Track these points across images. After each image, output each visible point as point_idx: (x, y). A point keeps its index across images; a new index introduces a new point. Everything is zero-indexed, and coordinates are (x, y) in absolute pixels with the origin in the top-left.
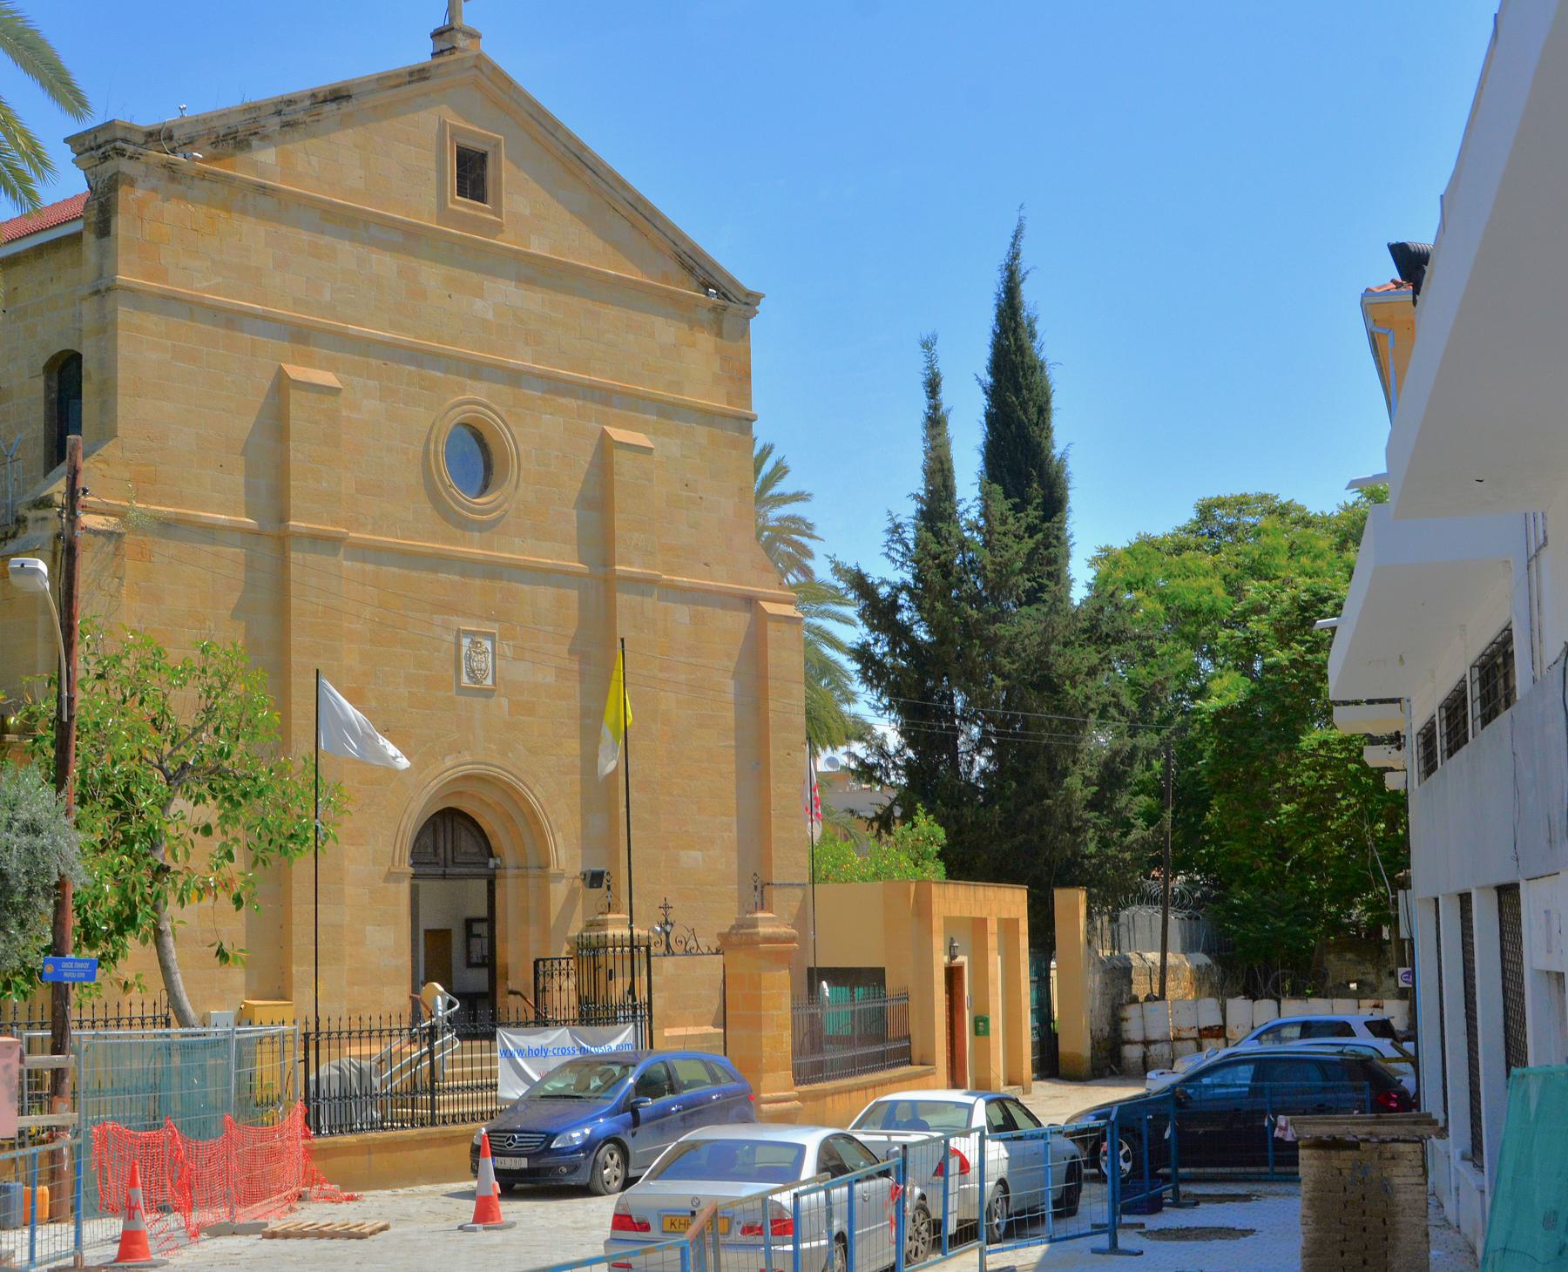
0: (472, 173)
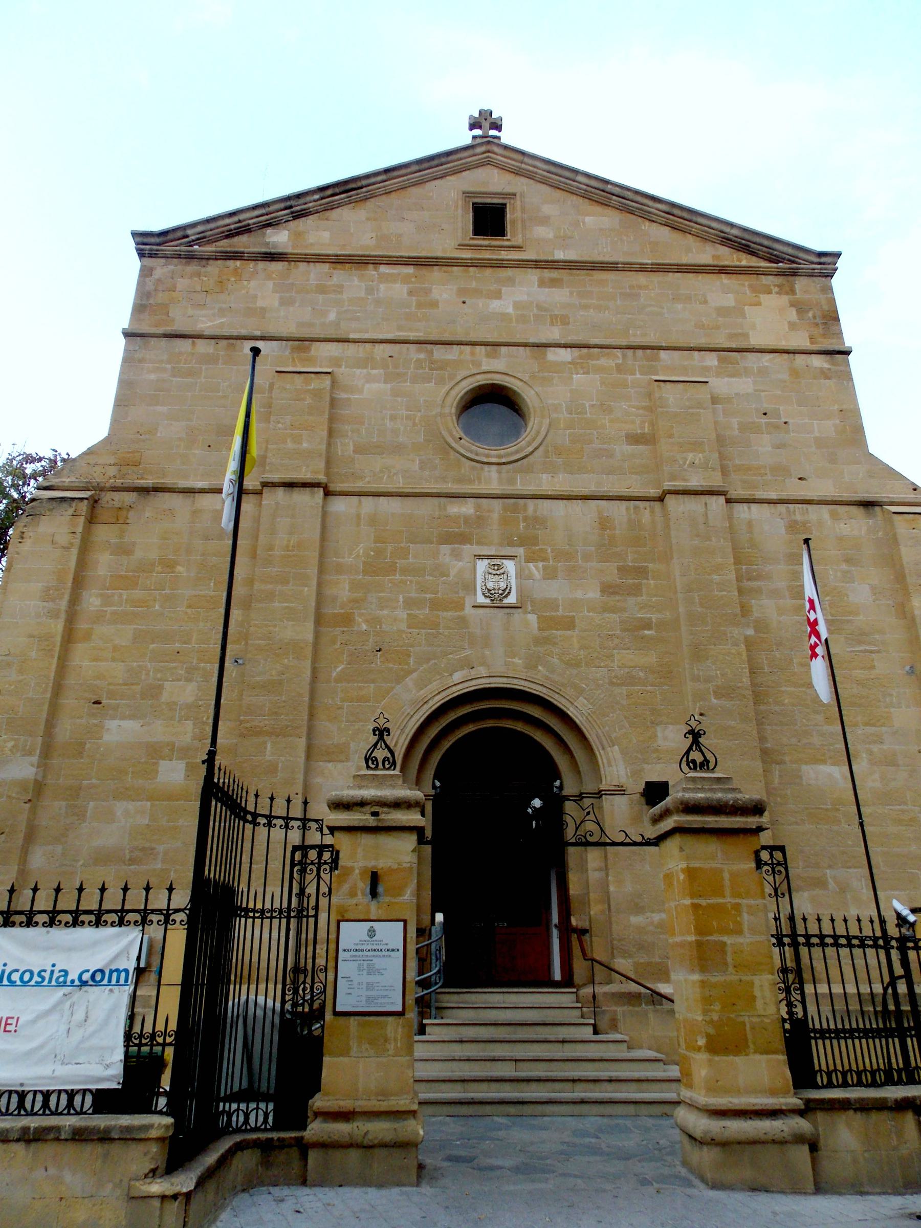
0: (489, 219)
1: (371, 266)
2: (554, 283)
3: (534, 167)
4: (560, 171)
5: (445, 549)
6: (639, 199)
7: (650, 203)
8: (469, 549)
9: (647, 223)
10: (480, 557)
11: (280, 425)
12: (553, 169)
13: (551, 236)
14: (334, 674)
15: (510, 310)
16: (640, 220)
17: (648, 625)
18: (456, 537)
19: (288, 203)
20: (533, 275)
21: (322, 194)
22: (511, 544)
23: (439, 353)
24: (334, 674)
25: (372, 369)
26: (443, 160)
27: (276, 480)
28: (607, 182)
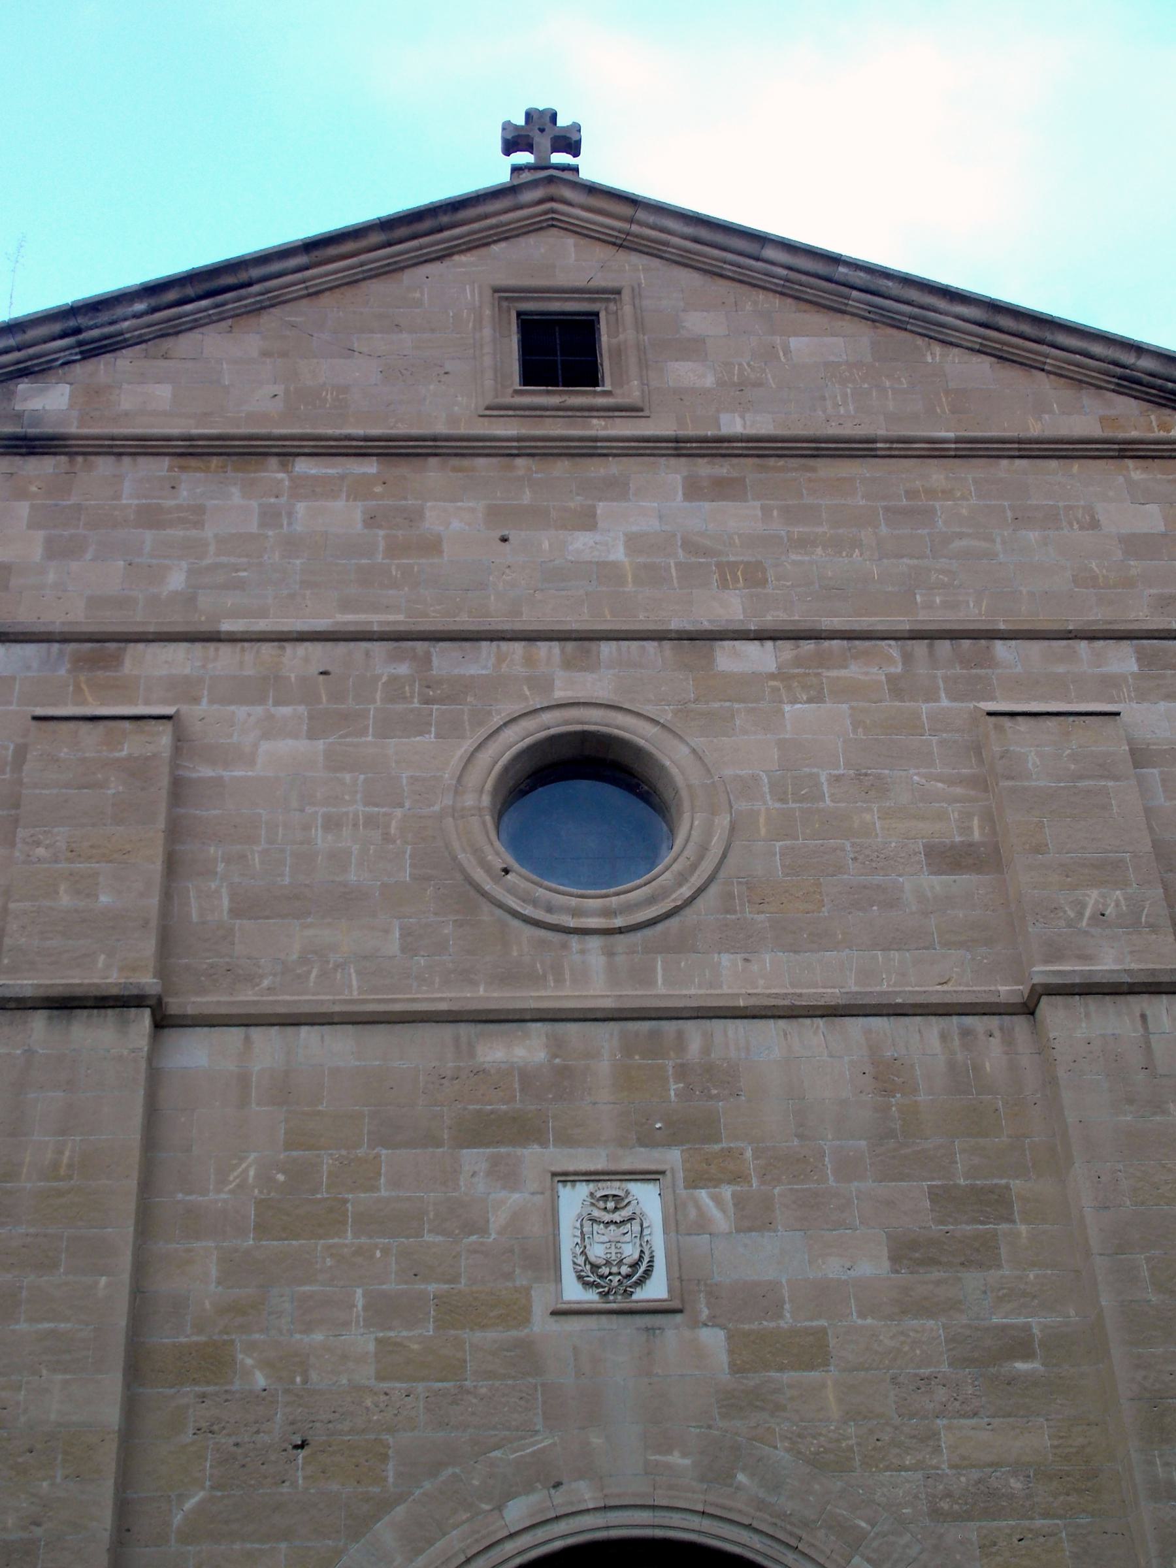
0: (559, 348)
1: (273, 462)
2: (723, 489)
3: (662, 230)
4: (719, 238)
5: (474, 1159)
6: (913, 294)
7: (942, 304)
8: (535, 1158)
9: (937, 349)
10: (566, 1177)
11: (41, 851)
12: (704, 233)
13: (709, 381)
14: (178, 1519)
15: (619, 554)
16: (919, 341)
17: (1019, 1345)
18: (503, 1127)
19: (72, 323)
20: (672, 474)
21: (153, 301)
22: (647, 1140)
23: (446, 661)
24: (178, 1519)
25: (277, 703)
26: (445, 219)
27: (29, 993)
28: (835, 260)
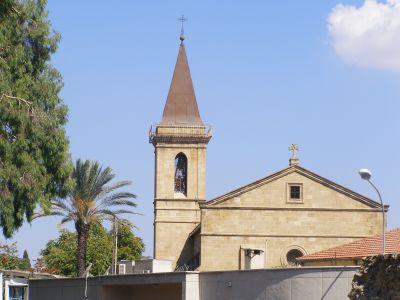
0: (295, 192)
2: (312, 215)
